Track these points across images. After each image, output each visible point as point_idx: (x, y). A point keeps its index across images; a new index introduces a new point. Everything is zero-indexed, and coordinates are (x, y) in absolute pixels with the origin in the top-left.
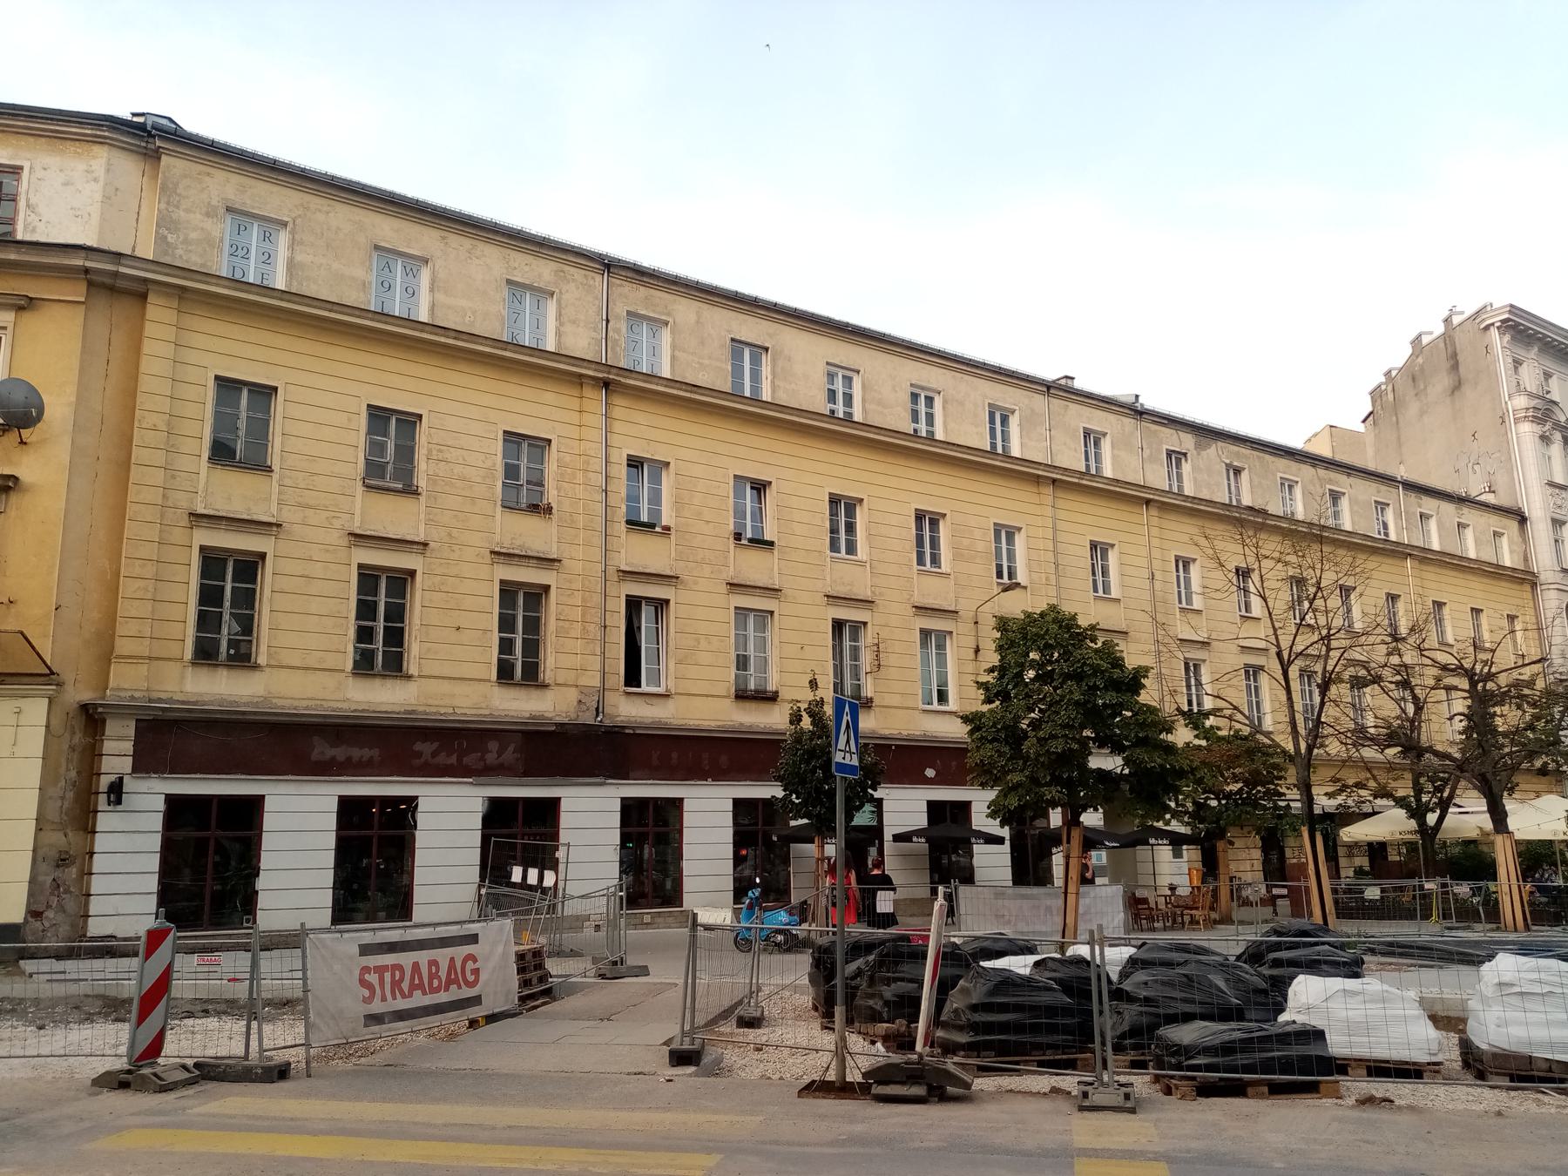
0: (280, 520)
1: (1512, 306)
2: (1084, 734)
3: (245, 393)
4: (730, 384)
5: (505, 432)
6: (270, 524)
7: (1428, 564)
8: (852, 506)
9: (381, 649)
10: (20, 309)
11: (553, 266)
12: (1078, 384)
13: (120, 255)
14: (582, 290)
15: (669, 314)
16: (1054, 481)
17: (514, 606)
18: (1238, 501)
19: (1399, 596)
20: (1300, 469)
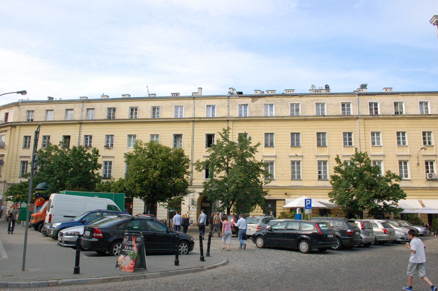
0: (436, 154)
1: (435, 16)
2: (211, 184)
3: (269, 135)
4: (420, 112)
5: (238, 134)
6: (29, 157)
7: (380, 119)
8: (350, 134)
9: (323, 175)
10: (6, 132)
11: (74, 104)
12: (89, 98)
13: (201, 118)
14: (77, 107)
15: (95, 107)
16: (193, 121)
17: (402, 164)
18: (246, 115)
19: (432, 132)
20: (301, 99)
